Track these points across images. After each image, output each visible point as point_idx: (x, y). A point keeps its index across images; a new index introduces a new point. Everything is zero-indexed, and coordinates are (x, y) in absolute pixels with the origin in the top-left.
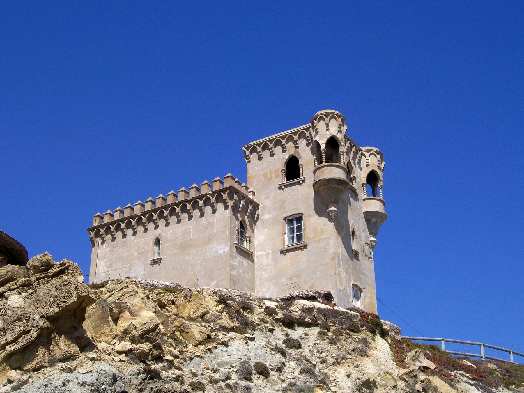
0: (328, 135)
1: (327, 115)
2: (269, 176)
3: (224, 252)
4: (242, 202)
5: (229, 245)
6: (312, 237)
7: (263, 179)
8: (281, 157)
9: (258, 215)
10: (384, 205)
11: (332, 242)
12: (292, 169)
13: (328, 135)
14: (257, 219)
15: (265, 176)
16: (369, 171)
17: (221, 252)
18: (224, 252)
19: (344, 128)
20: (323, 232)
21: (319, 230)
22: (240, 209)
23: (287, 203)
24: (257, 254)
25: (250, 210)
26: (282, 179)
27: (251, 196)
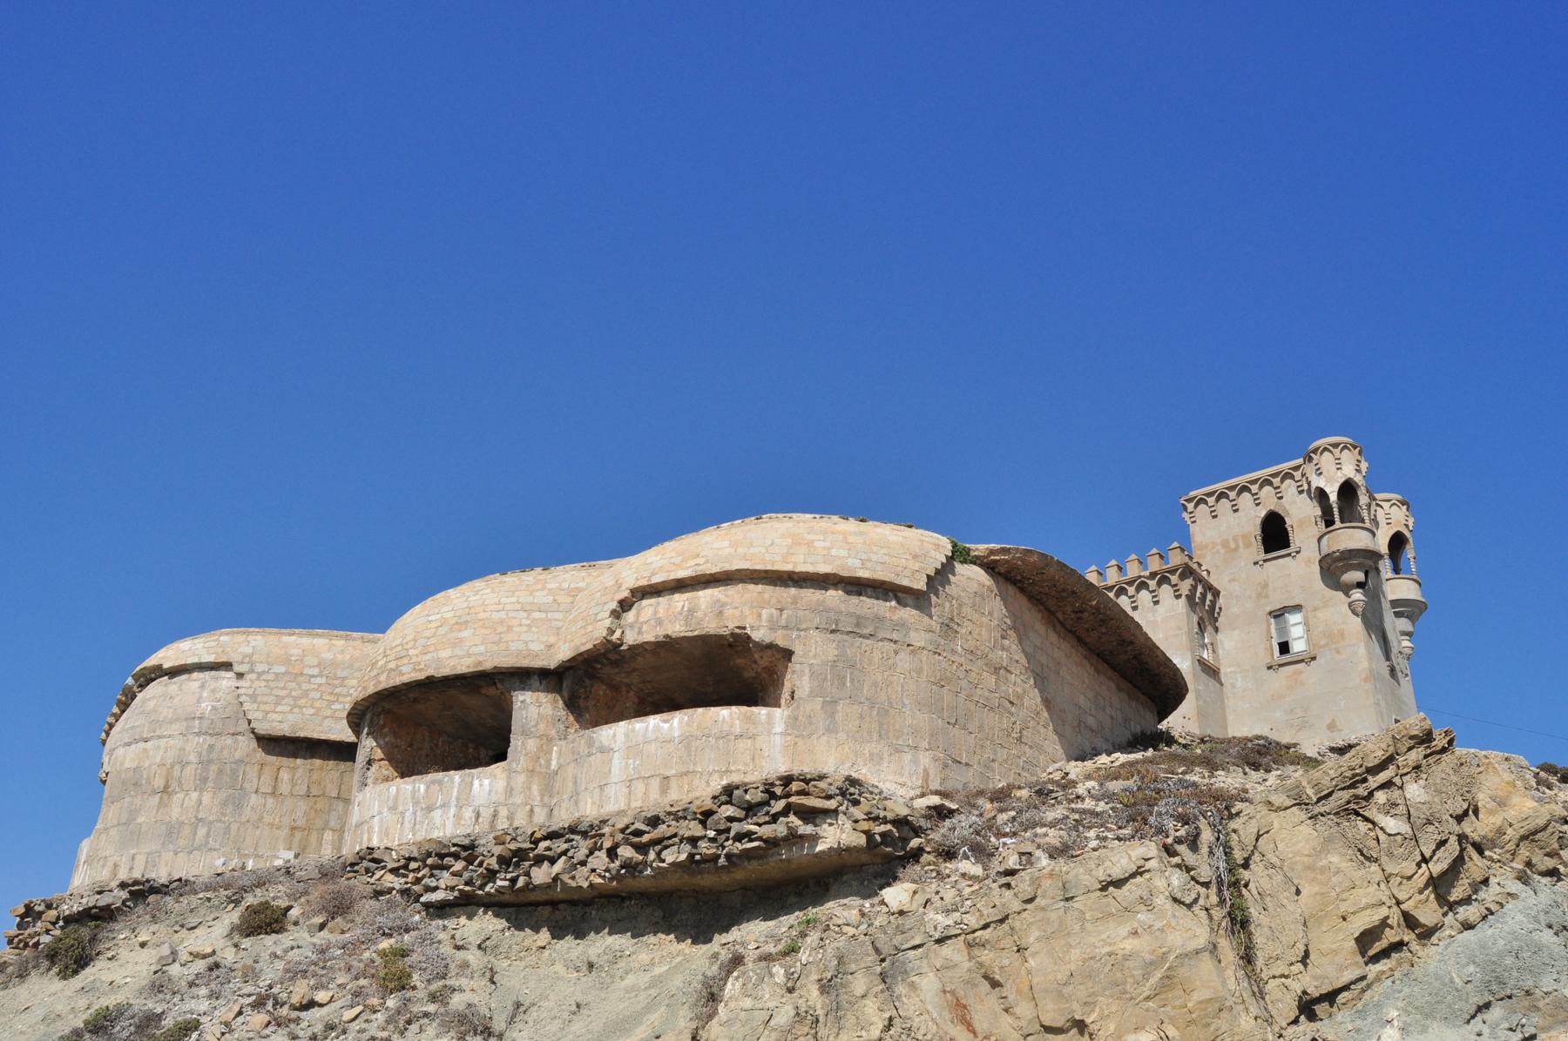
1: (1335, 445)
2: (1232, 545)
4: (1200, 589)
6: (1323, 643)
8: (1250, 516)
12: (1275, 534)
15: (1225, 544)
19: (1364, 466)
27: (1204, 574)
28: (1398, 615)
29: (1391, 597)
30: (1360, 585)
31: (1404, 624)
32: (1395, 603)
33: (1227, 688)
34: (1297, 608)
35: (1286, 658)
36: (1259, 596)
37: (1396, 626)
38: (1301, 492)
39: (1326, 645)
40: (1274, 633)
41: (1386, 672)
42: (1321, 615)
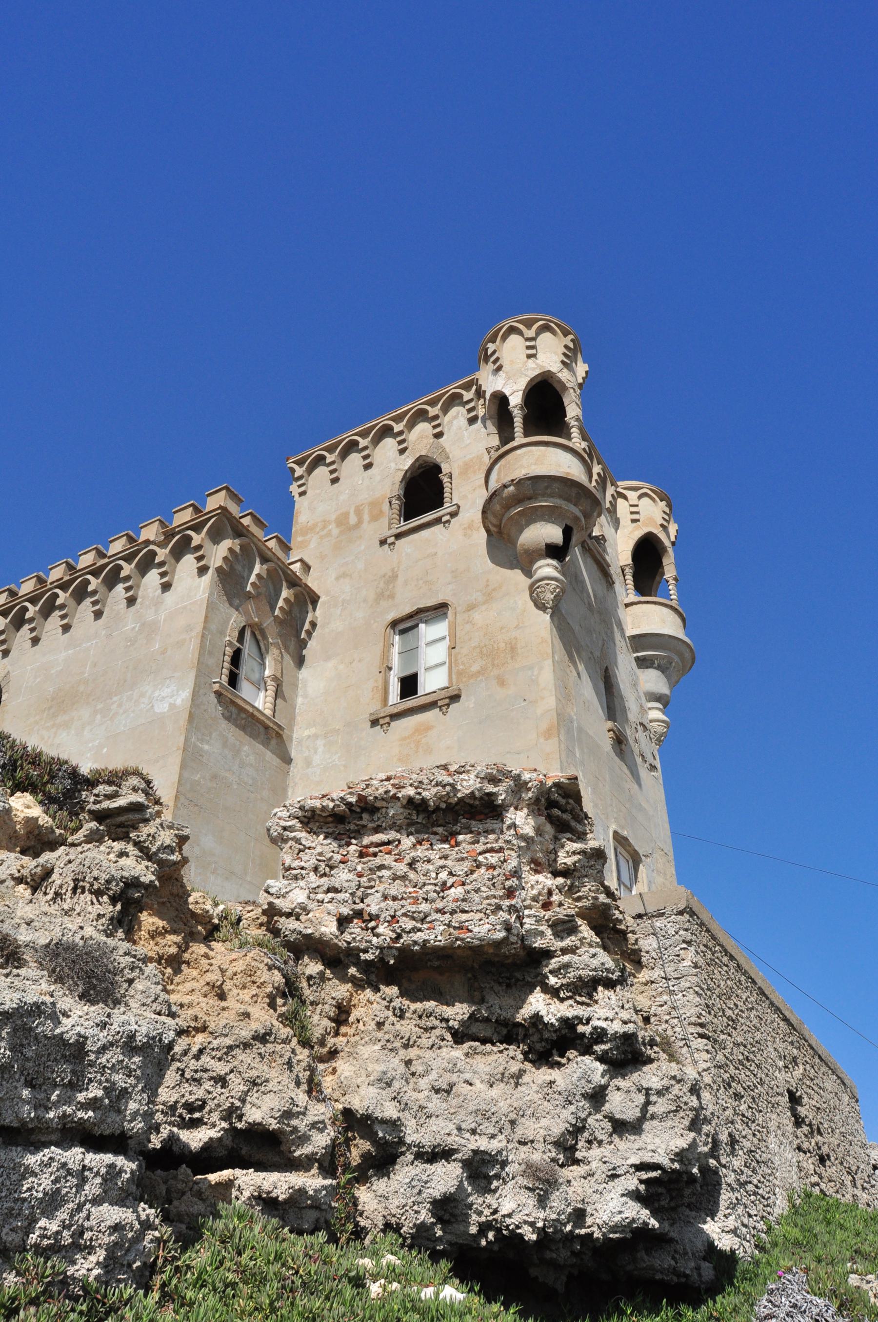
0: (532, 369)
3: (172, 706)
5: (191, 683)
6: (475, 668)
7: (335, 531)
8: (391, 464)
9: (314, 625)
10: (684, 620)
11: (547, 676)
13: (533, 369)
14: (309, 634)
16: (638, 534)
17: (162, 708)
18: (172, 706)
20: (513, 649)
21: (503, 645)
22: (249, 588)
23: (400, 580)
24: (301, 736)
25: (286, 600)
26: (388, 521)
28: (643, 663)
29: (631, 631)
30: (556, 552)
31: (653, 680)
32: (639, 641)
33: (296, 769)
34: (439, 610)
35: (411, 702)
36: (380, 596)
37: (641, 684)
38: (472, 421)
39: (482, 672)
40: (395, 660)
41: (606, 743)
42: (478, 617)
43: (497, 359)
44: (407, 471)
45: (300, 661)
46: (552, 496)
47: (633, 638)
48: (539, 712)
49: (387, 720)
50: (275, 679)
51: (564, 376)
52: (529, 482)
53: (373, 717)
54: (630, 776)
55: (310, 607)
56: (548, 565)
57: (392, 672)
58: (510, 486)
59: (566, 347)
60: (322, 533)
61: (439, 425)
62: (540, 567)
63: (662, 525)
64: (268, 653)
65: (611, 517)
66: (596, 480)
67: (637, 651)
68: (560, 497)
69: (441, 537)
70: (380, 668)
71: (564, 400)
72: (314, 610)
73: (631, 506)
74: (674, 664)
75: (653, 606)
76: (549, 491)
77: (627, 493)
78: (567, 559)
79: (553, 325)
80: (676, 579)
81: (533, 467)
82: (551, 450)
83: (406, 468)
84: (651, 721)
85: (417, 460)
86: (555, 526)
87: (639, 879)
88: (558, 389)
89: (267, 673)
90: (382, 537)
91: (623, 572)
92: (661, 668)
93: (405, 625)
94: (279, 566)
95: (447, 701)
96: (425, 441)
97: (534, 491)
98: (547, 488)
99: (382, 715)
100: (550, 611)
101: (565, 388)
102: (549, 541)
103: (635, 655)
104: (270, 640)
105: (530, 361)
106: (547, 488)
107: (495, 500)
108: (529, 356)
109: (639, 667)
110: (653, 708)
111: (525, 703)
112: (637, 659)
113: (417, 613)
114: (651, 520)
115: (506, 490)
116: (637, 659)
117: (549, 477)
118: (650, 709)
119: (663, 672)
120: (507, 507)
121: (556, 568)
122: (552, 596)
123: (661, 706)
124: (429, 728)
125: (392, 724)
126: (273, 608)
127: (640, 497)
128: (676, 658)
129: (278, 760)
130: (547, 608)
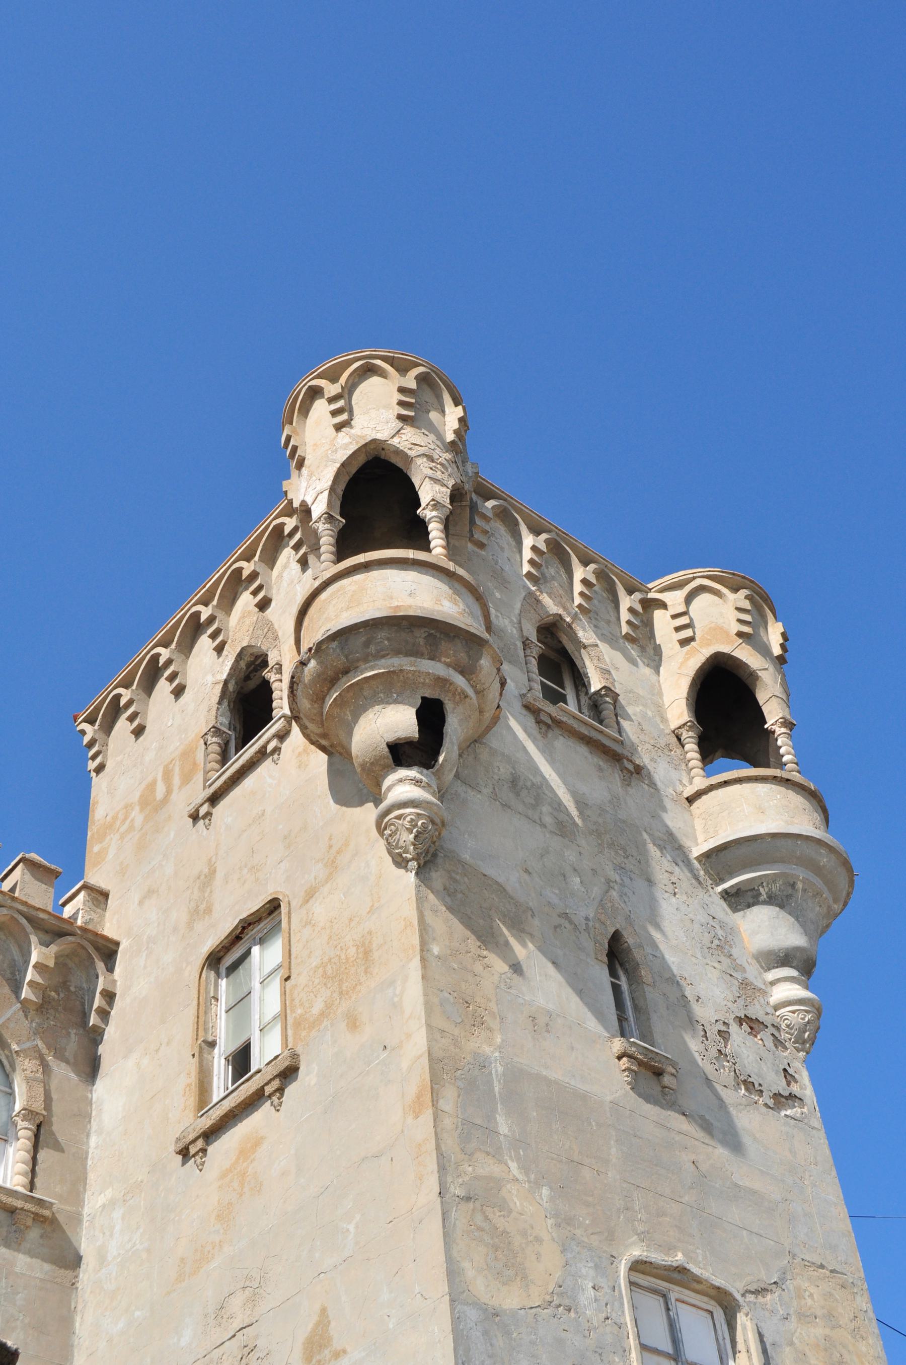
9: (110, 996)
14: (104, 1014)
21: (352, 951)
31: (765, 928)
32: (721, 859)
33: (87, 1274)
42: (320, 910)
43: (295, 449)
44: (226, 683)
45: (91, 1068)
46: (380, 655)
47: (707, 856)
48: (405, 1065)
49: (200, 1144)
50: (29, 1114)
51: (408, 440)
52: (334, 644)
53: (181, 1145)
54: (701, 1134)
55: (100, 966)
56: (401, 781)
57: (216, 1050)
58: (309, 660)
59: (402, 390)
60: (122, 829)
61: (260, 588)
62: (389, 789)
63: (740, 634)
64: (14, 1070)
65: (643, 649)
66: (582, 594)
67: (722, 880)
68: (398, 653)
69: (269, 780)
70: (192, 1046)
71: (413, 480)
72: (110, 969)
73: (674, 617)
74: (800, 885)
75: (737, 787)
76: (372, 649)
77: (665, 597)
78: (441, 759)
79: (378, 362)
80: (787, 724)
81: (345, 615)
82: (375, 574)
83: (224, 676)
84: (776, 1008)
85: (240, 656)
86: (401, 707)
87: (740, 1346)
88: (400, 465)
89: (18, 1107)
90: (191, 808)
91: (679, 739)
92: (779, 900)
93: (226, 958)
94: (20, 912)
95: (276, 1084)
96: (248, 621)
97: (346, 657)
98: (367, 644)
99: (191, 1137)
100: (413, 864)
101: (409, 460)
102: (391, 737)
103: (720, 889)
104: (15, 1047)
105: (341, 434)
106: (367, 644)
107: (299, 693)
108: (339, 427)
109: (735, 910)
110: (778, 981)
111: (385, 1054)
112: (726, 895)
113: (244, 928)
114: (717, 631)
115: (306, 669)
116: (726, 895)
117: (366, 624)
118: (773, 983)
119: (781, 906)
120: (320, 699)
121: (418, 782)
122: (412, 836)
123: (793, 973)
124: (256, 1142)
125: (211, 1149)
126: (16, 988)
127: (689, 599)
128: (801, 873)
129: (47, 1267)
130: (408, 861)
